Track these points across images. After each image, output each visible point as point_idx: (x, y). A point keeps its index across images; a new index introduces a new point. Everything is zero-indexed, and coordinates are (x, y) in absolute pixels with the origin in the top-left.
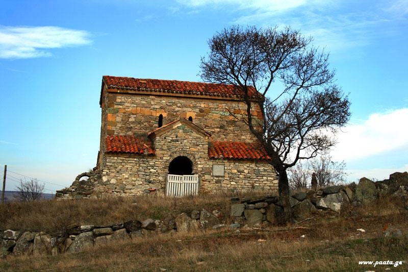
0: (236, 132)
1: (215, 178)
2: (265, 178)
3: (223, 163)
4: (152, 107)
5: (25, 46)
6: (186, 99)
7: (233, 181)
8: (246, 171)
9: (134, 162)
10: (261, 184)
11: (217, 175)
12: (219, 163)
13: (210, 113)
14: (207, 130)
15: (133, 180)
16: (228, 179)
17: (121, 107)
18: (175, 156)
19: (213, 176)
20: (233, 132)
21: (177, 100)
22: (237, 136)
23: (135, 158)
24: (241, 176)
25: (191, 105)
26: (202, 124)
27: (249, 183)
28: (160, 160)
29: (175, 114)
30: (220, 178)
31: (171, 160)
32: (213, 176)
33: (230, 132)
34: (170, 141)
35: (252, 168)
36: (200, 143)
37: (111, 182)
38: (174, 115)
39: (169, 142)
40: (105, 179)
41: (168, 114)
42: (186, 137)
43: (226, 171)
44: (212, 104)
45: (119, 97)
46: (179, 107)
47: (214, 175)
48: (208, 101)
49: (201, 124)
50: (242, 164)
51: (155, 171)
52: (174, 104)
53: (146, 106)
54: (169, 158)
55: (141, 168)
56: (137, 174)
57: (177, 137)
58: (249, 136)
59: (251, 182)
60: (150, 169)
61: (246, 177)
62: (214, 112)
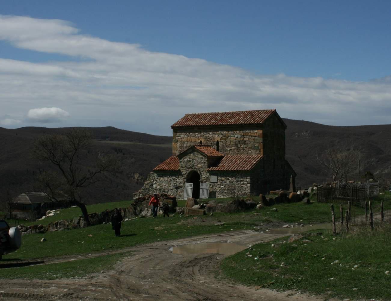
0: (245, 149)
1: (212, 184)
4: (196, 136)
7: (222, 186)
16: (219, 184)
19: (210, 182)
29: (209, 139)
30: (215, 184)
32: (210, 182)
36: (203, 162)
40: (154, 186)
43: (218, 179)
60: (176, 179)
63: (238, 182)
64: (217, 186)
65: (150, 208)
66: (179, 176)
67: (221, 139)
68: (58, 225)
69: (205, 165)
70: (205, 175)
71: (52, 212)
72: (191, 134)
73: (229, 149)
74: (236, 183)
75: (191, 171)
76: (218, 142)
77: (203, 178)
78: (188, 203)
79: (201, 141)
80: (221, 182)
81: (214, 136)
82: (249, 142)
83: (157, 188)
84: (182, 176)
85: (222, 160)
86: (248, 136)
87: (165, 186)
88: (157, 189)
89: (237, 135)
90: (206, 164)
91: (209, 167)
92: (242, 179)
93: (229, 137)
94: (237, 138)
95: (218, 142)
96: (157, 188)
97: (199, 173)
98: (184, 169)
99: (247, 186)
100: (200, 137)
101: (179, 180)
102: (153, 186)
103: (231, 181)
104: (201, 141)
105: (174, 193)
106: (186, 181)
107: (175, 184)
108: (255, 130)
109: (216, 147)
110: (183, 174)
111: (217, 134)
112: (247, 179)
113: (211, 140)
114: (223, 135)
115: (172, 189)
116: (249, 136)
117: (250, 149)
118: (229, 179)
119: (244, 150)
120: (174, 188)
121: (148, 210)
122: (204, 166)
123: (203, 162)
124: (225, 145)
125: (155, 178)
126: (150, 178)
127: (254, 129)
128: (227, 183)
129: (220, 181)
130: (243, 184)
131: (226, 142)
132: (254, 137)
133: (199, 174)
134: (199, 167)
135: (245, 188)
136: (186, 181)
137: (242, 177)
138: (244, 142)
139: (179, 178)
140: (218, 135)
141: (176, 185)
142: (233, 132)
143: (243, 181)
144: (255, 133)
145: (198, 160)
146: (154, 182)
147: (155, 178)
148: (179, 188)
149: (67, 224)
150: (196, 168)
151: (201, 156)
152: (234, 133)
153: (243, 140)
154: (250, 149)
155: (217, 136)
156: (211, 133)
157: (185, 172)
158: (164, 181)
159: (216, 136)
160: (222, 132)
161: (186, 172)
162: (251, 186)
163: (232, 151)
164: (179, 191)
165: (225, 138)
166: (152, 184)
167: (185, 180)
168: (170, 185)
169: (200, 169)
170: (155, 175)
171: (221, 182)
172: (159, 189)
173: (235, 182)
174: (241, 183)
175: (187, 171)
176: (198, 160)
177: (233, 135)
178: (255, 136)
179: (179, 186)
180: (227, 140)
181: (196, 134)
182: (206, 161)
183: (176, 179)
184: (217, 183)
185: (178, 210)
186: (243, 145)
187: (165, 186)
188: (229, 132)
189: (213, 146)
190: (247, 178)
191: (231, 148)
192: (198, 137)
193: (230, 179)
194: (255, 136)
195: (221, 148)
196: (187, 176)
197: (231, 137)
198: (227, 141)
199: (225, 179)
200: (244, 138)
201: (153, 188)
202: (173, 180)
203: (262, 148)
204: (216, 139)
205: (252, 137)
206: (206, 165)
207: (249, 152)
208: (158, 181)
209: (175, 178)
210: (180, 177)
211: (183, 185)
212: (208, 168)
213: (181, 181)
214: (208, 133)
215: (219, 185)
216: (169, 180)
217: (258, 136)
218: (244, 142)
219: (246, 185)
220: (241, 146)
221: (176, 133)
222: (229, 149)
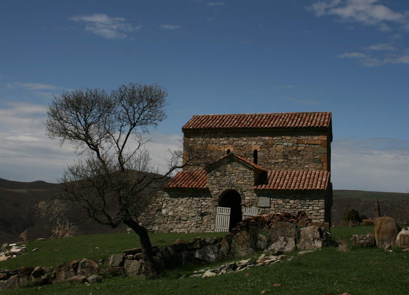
1: (261, 209)
4: (222, 143)
16: (274, 209)
19: (259, 207)
29: (241, 148)
32: (259, 207)
36: (247, 177)
37: (169, 214)
38: (240, 149)
40: (164, 211)
60: (202, 202)
63: (303, 206)
65: (291, 237)
66: (206, 197)
67: (261, 148)
68: (79, 268)
69: (250, 182)
70: (249, 196)
71: (12, 246)
72: (213, 139)
73: (273, 161)
74: (301, 208)
76: (256, 151)
77: (246, 201)
78: (382, 226)
79: (229, 151)
80: (276, 206)
81: (250, 143)
82: (305, 153)
83: (169, 214)
84: (211, 197)
85: (267, 176)
86: (304, 144)
87: (183, 211)
88: (168, 216)
89: (288, 142)
90: (251, 180)
91: (256, 184)
92: (311, 203)
93: (274, 144)
94: (287, 146)
95: (256, 151)
96: (169, 214)
97: (240, 193)
98: (215, 186)
99: (318, 213)
100: (227, 144)
101: (206, 203)
104: (229, 151)
105: (197, 222)
106: (218, 204)
107: (200, 209)
108: (316, 136)
109: (253, 158)
110: (212, 194)
111: (255, 140)
112: (320, 203)
113: (246, 148)
114: (264, 142)
115: (194, 216)
116: (306, 144)
117: (308, 162)
118: (289, 203)
119: (298, 163)
120: (197, 214)
121: (285, 240)
122: (249, 183)
123: (247, 177)
124: (268, 156)
126: (157, 199)
127: (313, 135)
128: (286, 208)
129: (275, 205)
130: (313, 210)
131: (269, 152)
132: (313, 146)
133: (240, 195)
134: (240, 184)
135: (316, 216)
136: (218, 204)
137: (311, 200)
138: (297, 153)
139: (206, 200)
140: (257, 143)
141: (202, 211)
142: (281, 139)
143: (313, 206)
144: (315, 140)
145: (239, 174)
147: (165, 200)
148: (205, 215)
149: (97, 266)
150: (235, 185)
151: (244, 169)
152: (282, 139)
153: (295, 149)
154: (308, 162)
155: (255, 144)
156: (245, 139)
157: (216, 191)
158: (182, 204)
159: (254, 143)
160: (262, 138)
161: (218, 191)
162: (325, 213)
163: (279, 164)
164: (205, 219)
165: (267, 146)
166: (161, 209)
167: (217, 203)
168: (191, 211)
169: (241, 188)
170: (166, 195)
171: (276, 206)
172: (172, 216)
173: (300, 207)
174: (308, 208)
175: (219, 190)
176: (239, 174)
177: (281, 142)
178: (315, 145)
179: (205, 212)
180: (270, 149)
181: (221, 139)
182: (252, 176)
183: (201, 201)
185: (360, 240)
186: (297, 157)
187: (183, 211)
188: (274, 138)
189: (249, 157)
190: (318, 202)
191: (277, 161)
192: (225, 144)
193: (292, 202)
194: (315, 145)
195: (262, 160)
196: (220, 197)
197: (277, 145)
198: (270, 151)
199: (283, 202)
200: (298, 146)
201: (162, 215)
202: (196, 203)
203: (326, 161)
204: (252, 148)
205: (310, 146)
206: (252, 182)
207: (306, 166)
208: (171, 204)
209: (199, 200)
210: (207, 198)
211: (212, 210)
212: (256, 187)
213: (210, 204)
214: (240, 139)
215: (272, 210)
216: (188, 203)
217: (320, 144)
218: (297, 153)
219: (318, 211)
220: (293, 158)
221: (189, 137)
222: (273, 161)
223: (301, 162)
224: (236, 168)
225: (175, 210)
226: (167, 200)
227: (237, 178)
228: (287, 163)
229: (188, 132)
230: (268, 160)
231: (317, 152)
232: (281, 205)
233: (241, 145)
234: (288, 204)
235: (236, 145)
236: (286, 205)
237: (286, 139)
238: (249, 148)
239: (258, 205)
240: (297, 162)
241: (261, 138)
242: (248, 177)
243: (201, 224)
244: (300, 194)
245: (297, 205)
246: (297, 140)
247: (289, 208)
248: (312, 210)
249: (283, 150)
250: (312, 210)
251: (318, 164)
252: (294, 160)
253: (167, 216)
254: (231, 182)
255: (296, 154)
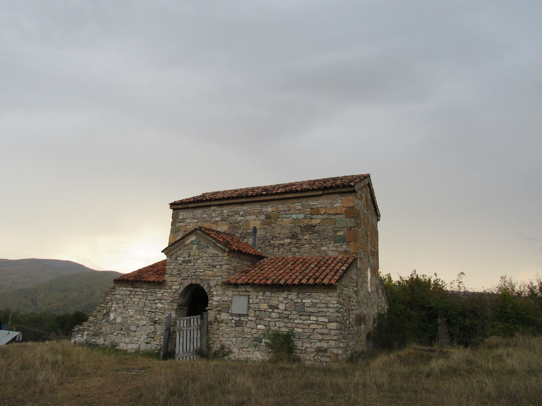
0: (313, 241)
1: (235, 318)
2: (313, 318)
3: (248, 294)
4: (214, 219)
5: (256, 191)
6: (250, 204)
7: (260, 324)
8: (282, 306)
9: (141, 293)
10: (306, 330)
11: (237, 312)
12: (241, 293)
13: (279, 218)
14: (274, 242)
15: (137, 319)
16: (254, 319)
17: (182, 224)
18: (187, 283)
19: (231, 315)
20: (310, 242)
21: (240, 208)
22: (315, 247)
23: (142, 288)
24: (274, 315)
25: (256, 211)
26: (268, 235)
27: (285, 327)
28: (169, 291)
29: (237, 225)
30: (242, 318)
31: (182, 289)
32: (231, 315)
33: (305, 242)
34: (181, 262)
35: (292, 300)
36: (217, 263)
37: (117, 321)
38: (236, 227)
39: (180, 264)
40: (112, 316)
41: (230, 226)
42: (201, 254)
43: (251, 306)
44: (281, 206)
45: (182, 213)
46: (242, 216)
47: (233, 312)
48: (276, 202)
49: (267, 235)
50: (275, 295)
51: (162, 306)
52: (237, 213)
53: (206, 219)
54: (178, 287)
55: (147, 302)
56: (141, 312)
57: (189, 256)
58: (332, 245)
59: (289, 325)
60: (157, 303)
61: (281, 317)
62: (283, 216)
64: (248, 325)
75: (191, 285)
76: (255, 229)
77: (215, 303)
86: (321, 214)
94: (297, 219)
95: (255, 229)
102: (109, 315)
103: (285, 312)
107: (153, 314)
118: (277, 308)
123: (217, 263)
125: (116, 298)
146: (113, 308)
150: (201, 278)
172: (120, 324)
174: (309, 320)
184: (247, 315)
191: (282, 242)
201: (108, 321)
204: (251, 224)
213: (166, 306)
220: (305, 237)
223: (315, 243)
224: (204, 249)
225: (124, 315)
226: (117, 300)
227: (204, 266)
228: (296, 244)
229: (177, 206)
230: (270, 242)
231: (339, 226)
232: (265, 311)
233: (237, 221)
234: (275, 310)
235: (231, 221)
236: (273, 312)
237: (294, 209)
238: (246, 225)
239: (230, 311)
240: (310, 242)
241: (261, 210)
242: (220, 264)
243: (153, 338)
244: (296, 293)
245: (289, 313)
246: (310, 210)
247: (276, 318)
248: (315, 322)
249: (291, 225)
250: (315, 322)
251: (341, 244)
252: (306, 239)
253: (115, 322)
254: (196, 271)
255: (309, 229)
